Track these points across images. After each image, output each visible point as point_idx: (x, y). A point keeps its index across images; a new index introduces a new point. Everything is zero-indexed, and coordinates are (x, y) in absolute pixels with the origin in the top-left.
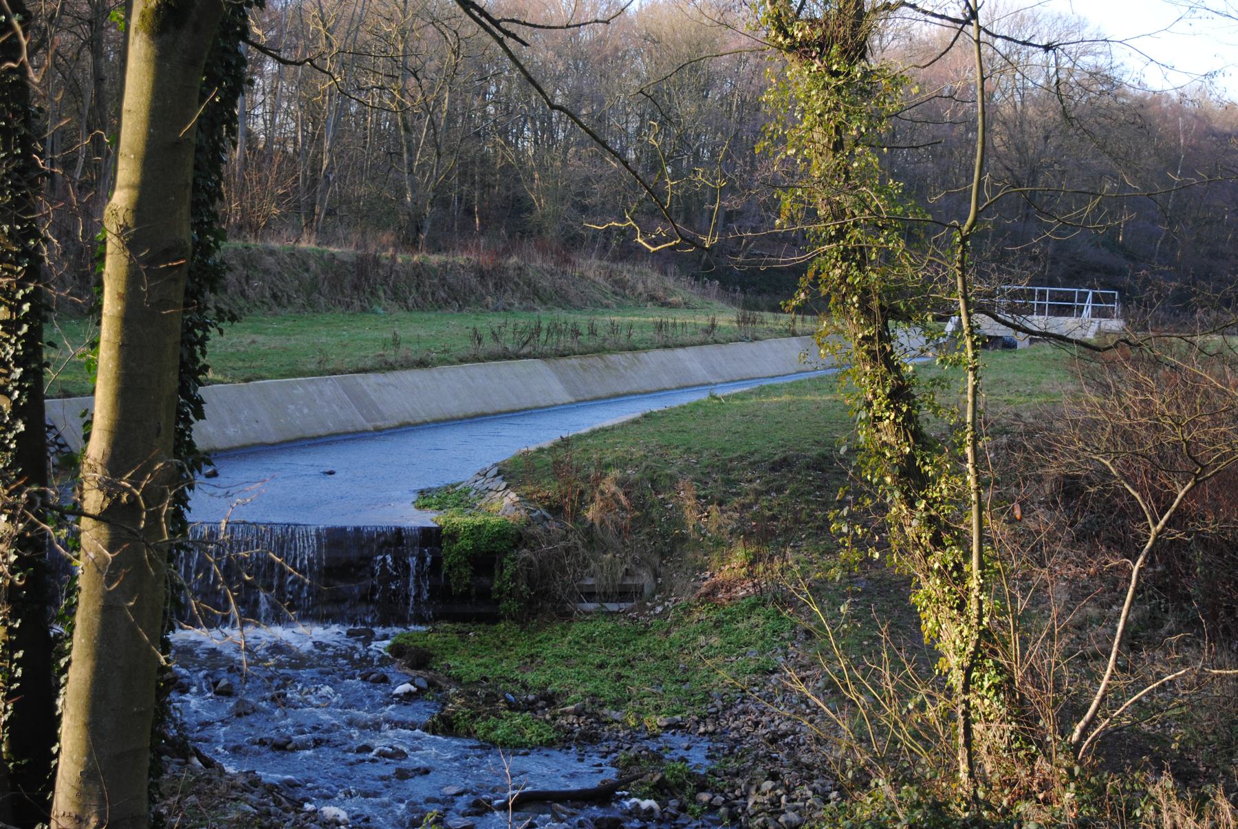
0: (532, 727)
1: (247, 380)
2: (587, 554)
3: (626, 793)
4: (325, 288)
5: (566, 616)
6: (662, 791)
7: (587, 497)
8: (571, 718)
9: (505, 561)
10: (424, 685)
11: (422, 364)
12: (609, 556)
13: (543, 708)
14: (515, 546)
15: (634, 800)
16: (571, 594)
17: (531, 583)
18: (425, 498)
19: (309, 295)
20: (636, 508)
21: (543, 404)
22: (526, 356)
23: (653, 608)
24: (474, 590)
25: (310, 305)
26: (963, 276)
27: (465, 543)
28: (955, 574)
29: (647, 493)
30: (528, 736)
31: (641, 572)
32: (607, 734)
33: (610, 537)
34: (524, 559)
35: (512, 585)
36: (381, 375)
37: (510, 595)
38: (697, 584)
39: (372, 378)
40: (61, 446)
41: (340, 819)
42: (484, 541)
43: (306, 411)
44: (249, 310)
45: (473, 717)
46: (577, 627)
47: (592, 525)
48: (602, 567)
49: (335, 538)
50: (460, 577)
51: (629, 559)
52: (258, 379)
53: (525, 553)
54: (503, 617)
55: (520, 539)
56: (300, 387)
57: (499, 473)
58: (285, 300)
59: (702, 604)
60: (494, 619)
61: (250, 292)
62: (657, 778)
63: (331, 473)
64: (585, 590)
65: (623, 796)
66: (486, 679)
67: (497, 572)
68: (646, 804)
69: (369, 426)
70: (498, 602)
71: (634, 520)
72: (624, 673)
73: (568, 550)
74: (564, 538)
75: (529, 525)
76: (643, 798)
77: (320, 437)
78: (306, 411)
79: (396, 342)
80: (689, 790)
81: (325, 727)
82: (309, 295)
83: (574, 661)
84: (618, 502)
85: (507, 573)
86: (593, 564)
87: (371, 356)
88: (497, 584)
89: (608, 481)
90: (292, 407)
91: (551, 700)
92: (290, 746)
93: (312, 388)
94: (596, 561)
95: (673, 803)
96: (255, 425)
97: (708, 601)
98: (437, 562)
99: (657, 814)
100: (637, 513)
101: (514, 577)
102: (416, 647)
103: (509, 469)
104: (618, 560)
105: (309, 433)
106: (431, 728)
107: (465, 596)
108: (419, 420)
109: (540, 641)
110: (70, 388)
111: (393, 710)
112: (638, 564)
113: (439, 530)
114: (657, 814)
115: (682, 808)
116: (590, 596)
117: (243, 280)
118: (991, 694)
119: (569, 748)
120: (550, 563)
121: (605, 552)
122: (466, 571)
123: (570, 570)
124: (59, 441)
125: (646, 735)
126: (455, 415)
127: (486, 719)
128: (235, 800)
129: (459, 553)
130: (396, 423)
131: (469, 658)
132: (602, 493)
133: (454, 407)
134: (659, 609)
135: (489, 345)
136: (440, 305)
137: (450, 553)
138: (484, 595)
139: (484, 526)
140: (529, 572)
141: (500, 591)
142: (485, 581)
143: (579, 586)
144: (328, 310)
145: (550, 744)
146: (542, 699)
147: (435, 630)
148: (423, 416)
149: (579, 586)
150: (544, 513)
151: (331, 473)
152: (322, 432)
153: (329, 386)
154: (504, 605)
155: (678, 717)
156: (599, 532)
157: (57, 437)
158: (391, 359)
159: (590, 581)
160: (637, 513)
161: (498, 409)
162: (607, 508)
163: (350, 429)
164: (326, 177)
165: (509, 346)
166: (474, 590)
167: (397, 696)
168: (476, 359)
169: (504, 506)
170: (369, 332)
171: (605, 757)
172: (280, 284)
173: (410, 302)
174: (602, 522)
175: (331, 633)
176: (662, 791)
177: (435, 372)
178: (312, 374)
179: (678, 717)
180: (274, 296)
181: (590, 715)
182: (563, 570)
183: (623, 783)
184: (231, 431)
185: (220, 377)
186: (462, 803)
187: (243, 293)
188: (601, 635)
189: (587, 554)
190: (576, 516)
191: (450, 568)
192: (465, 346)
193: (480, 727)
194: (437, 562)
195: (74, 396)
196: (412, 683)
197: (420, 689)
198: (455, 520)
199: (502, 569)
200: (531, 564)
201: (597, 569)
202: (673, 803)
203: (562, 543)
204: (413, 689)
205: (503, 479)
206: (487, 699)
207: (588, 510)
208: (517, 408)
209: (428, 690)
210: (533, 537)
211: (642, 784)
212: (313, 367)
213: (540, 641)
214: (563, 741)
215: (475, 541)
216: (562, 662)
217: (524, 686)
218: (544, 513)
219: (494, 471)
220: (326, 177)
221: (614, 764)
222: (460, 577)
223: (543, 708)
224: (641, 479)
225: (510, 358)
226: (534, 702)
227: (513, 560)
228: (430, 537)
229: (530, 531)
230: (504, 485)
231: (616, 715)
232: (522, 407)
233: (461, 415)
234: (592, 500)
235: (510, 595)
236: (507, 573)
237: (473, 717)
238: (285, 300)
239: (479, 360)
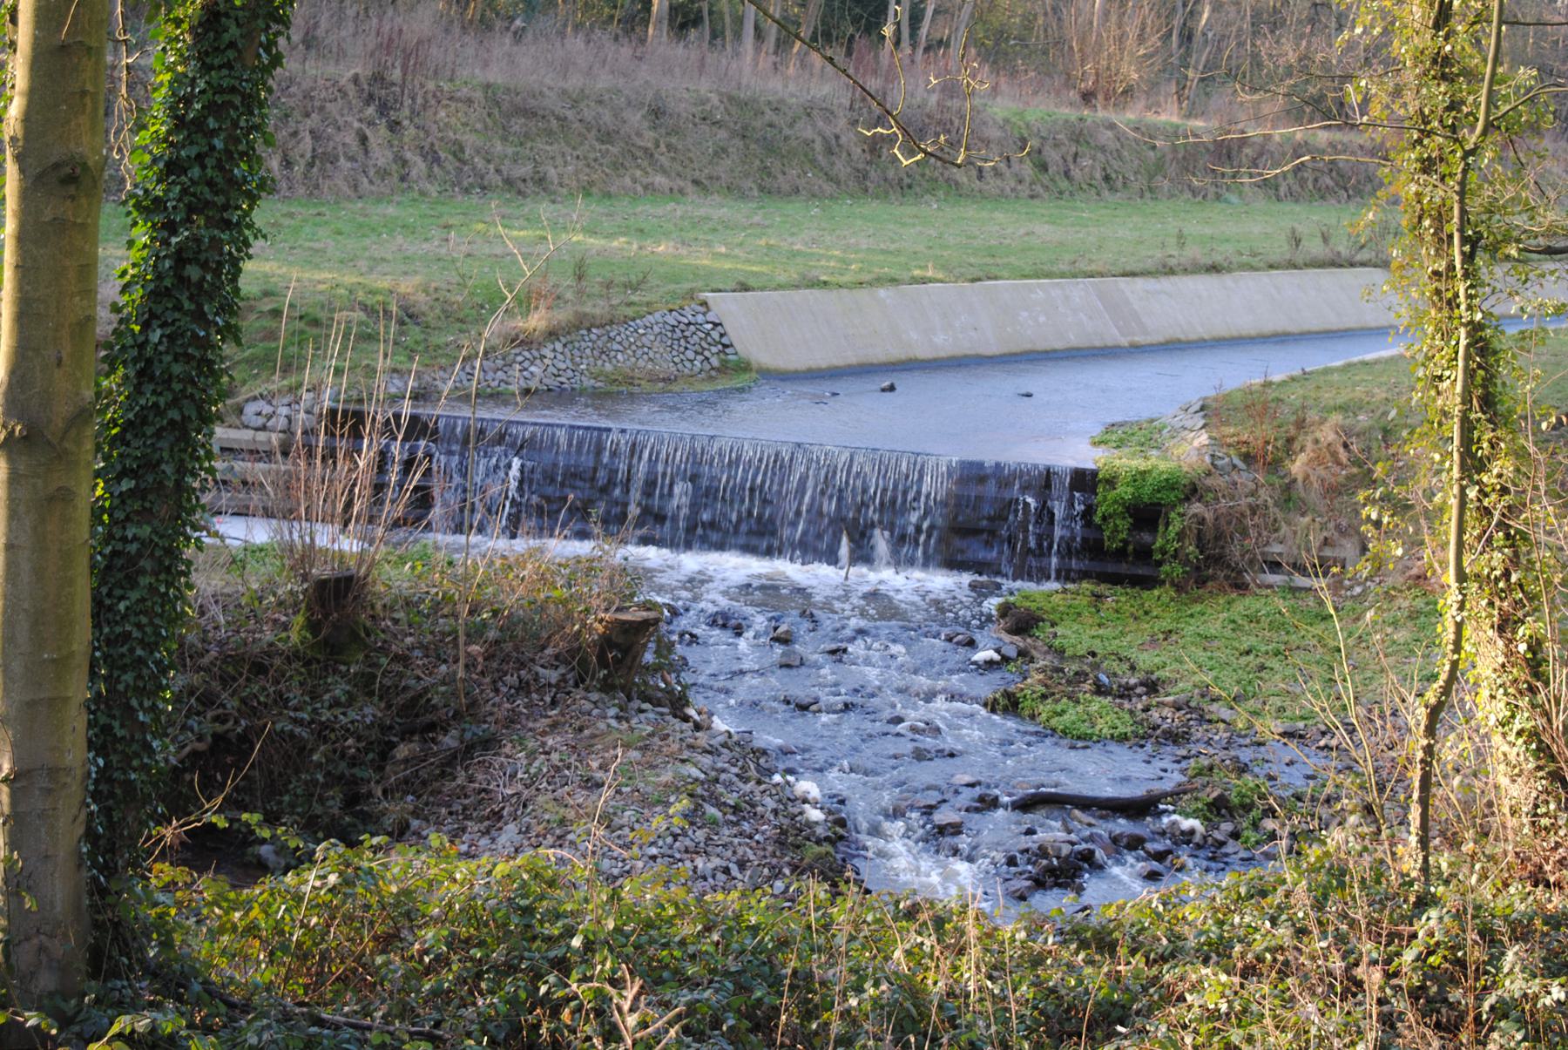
0: (1104, 714)
1: (974, 280)
2: (1279, 515)
3: (1171, 808)
4: (1172, 170)
5: (1241, 587)
6: (1219, 810)
7: (1297, 446)
8: (1167, 712)
9: (1172, 515)
10: (1012, 653)
11: (1214, 269)
12: (1307, 519)
13: (1140, 696)
14: (1187, 499)
15: (1175, 817)
16: (1251, 562)
17: (1201, 547)
18: (1115, 435)
19: (1151, 177)
20: (1354, 464)
21: (1373, 324)
22: (1363, 264)
23: (1351, 588)
24: (1131, 548)
25: (1151, 190)
26: (1461, 202)
27: (1124, 491)
28: (1501, 585)
29: (1374, 445)
30: (1098, 728)
31: (1344, 541)
32: (1199, 735)
33: (1314, 496)
34: (1195, 515)
35: (1176, 545)
36: (1152, 280)
37: (1175, 556)
38: (1409, 564)
39: (1139, 283)
40: (725, 346)
41: (810, 797)
42: (1147, 490)
43: (1042, 319)
44: (1071, 194)
45: (1044, 697)
46: (1247, 601)
47: (1295, 481)
48: (1295, 533)
49: (972, 474)
50: (1116, 530)
51: (1331, 525)
52: (989, 278)
53: (1197, 508)
54: (1162, 583)
55: (1194, 490)
56: (1040, 289)
57: (1202, 409)
58: (1119, 184)
59: (1409, 589)
60: (1148, 583)
61: (1076, 173)
62: (1215, 794)
63: (1029, 395)
64: (1270, 558)
65: (1165, 811)
66: (1094, 654)
67: (1161, 528)
68: (1188, 824)
69: (1124, 342)
70: (1160, 563)
71: (1349, 478)
72: (1268, 664)
73: (1254, 510)
74: (1253, 494)
75: (1209, 474)
76: (1187, 816)
77: (1055, 351)
78: (1042, 319)
79: (1181, 239)
80: (1254, 813)
81: (869, 690)
82: (1151, 177)
83: (1216, 643)
84: (1334, 454)
85: (1173, 530)
86: (1284, 529)
87: (1152, 255)
88: (1159, 542)
89: (1326, 427)
90: (1025, 314)
91: (1152, 687)
92: (814, 708)
93: (1056, 293)
94: (1289, 523)
95: (1227, 827)
96: (973, 333)
97: (1416, 586)
98: (1089, 511)
99: (1197, 838)
100: (1355, 470)
101: (1181, 536)
102: (1027, 609)
103: (1214, 405)
104: (1317, 526)
105: (1041, 345)
106: (992, 707)
107: (1120, 554)
108: (1193, 337)
109: (1192, 616)
110: (752, 282)
111: (962, 680)
112: (1342, 532)
113: (1094, 473)
114: (1197, 838)
115: (1235, 835)
116: (1275, 566)
117: (1070, 159)
118: (1521, 741)
119: (1142, 746)
120: (1229, 523)
121: (1303, 515)
122: (1124, 524)
123: (1253, 533)
124: (725, 340)
125: (1248, 741)
126: (1244, 333)
127: (1057, 701)
128: (683, 761)
129: (1115, 502)
130: (1161, 339)
131: (1085, 623)
132: (1317, 441)
133: (1245, 324)
134: (1358, 590)
135: (1315, 247)
136: (1322, 194)
137: (1106, 500)
138: (1144, 554)
139: (1150, 472)
140: (1199, 531)
141: (1163, 552)
142: (1146, 537)
143: (1263, 554)
144: (1171, 196)
145: (1122, 739)
146: (1142, 684)
147: (1065, 591)
148: (1200, 331)
149: (1263, 554)
150: (1237, 461)
151: (1029, 395)
152: (1059, 345)
153: (1079, 290)
154: (1166, 568)
155: (1301, 724)
156: (1301, 490)
157: (722, 335)
158: (1172, 262)
159: (1276, 548)
160: (1355, 470)
161: (1306, 327)
162: (1317, 460)
163: (1098, 343)
164: (1204, 34)
165: (1341, 249)
166: (1131, 548)
167: (975, 663)
168: (1292, 265)
169: (1189, 450)
170: (1123, 228)
171: (1178, 762)
172: (1116, 164)
173: (1283, 190)
174: (1307, 477)
175: (941, 582)
176: (1219, 810)
177: (1227, 279)
178: (1063, 275)
179: (1301, 724)
180: (1107, 178)
181: (1192, 710)
182: (1244, 533)
183: (1176, 794)
184: (939, 339)
185: (940, 276)
186: (967, 796)
187: (1067, 174)
188: (1268, 615)
189: (1279, 515)
190: (1274, 465)
191: (1104, 518)
192: (1279, 249)
193: (1044, 709)
194: (1089, 511)
195: (753, 289)
196: (998, 651)
197: (1006, 659)
198: (1117, 463)
199: (1167, 524)
200: (1202, 521)
201: (1290, 534)
202: (1227, 827)
203: (1250, 500)
204: (997, 657)
205: (1205, 416)
206: (1081, 677)
207: (1293, 462)
208: (1335, 327)
209: (1015, 660)
210: (1209, 490)
211: (1196, 799)
212: (1064, 267)
213: (1192, 616)
214: (1146, 736)
215: (1137, 489)
216: (1185, 645)
217: (1133, 668)
218: (1237, 461)
219: (1197, 407)
220: (1204, 34)
221: (1183, 771)
222: (1116, 530)
223: (1140, 696)
224: (1371, 428)
225: (1341, 266)
226: (1133, 688)
227: (1182, 515)
228: (1084, 480)
229: (1209, 482)
230: (1202, 423)
231: (1225, 714)
232: (1342, 326)
233: (1253, 333)
234: (1302, 449)
235: (1175, 556)
236: (1173, 530)
237: (1044, 697)
238: (1119, 184)
239: (1295, 267)
